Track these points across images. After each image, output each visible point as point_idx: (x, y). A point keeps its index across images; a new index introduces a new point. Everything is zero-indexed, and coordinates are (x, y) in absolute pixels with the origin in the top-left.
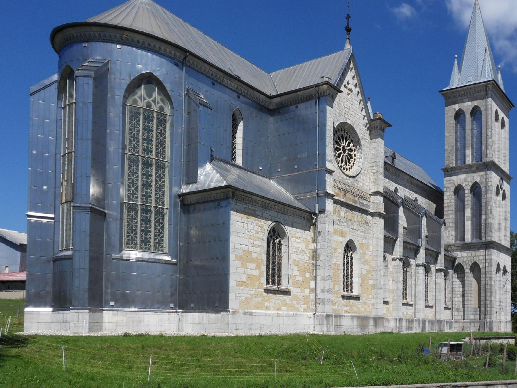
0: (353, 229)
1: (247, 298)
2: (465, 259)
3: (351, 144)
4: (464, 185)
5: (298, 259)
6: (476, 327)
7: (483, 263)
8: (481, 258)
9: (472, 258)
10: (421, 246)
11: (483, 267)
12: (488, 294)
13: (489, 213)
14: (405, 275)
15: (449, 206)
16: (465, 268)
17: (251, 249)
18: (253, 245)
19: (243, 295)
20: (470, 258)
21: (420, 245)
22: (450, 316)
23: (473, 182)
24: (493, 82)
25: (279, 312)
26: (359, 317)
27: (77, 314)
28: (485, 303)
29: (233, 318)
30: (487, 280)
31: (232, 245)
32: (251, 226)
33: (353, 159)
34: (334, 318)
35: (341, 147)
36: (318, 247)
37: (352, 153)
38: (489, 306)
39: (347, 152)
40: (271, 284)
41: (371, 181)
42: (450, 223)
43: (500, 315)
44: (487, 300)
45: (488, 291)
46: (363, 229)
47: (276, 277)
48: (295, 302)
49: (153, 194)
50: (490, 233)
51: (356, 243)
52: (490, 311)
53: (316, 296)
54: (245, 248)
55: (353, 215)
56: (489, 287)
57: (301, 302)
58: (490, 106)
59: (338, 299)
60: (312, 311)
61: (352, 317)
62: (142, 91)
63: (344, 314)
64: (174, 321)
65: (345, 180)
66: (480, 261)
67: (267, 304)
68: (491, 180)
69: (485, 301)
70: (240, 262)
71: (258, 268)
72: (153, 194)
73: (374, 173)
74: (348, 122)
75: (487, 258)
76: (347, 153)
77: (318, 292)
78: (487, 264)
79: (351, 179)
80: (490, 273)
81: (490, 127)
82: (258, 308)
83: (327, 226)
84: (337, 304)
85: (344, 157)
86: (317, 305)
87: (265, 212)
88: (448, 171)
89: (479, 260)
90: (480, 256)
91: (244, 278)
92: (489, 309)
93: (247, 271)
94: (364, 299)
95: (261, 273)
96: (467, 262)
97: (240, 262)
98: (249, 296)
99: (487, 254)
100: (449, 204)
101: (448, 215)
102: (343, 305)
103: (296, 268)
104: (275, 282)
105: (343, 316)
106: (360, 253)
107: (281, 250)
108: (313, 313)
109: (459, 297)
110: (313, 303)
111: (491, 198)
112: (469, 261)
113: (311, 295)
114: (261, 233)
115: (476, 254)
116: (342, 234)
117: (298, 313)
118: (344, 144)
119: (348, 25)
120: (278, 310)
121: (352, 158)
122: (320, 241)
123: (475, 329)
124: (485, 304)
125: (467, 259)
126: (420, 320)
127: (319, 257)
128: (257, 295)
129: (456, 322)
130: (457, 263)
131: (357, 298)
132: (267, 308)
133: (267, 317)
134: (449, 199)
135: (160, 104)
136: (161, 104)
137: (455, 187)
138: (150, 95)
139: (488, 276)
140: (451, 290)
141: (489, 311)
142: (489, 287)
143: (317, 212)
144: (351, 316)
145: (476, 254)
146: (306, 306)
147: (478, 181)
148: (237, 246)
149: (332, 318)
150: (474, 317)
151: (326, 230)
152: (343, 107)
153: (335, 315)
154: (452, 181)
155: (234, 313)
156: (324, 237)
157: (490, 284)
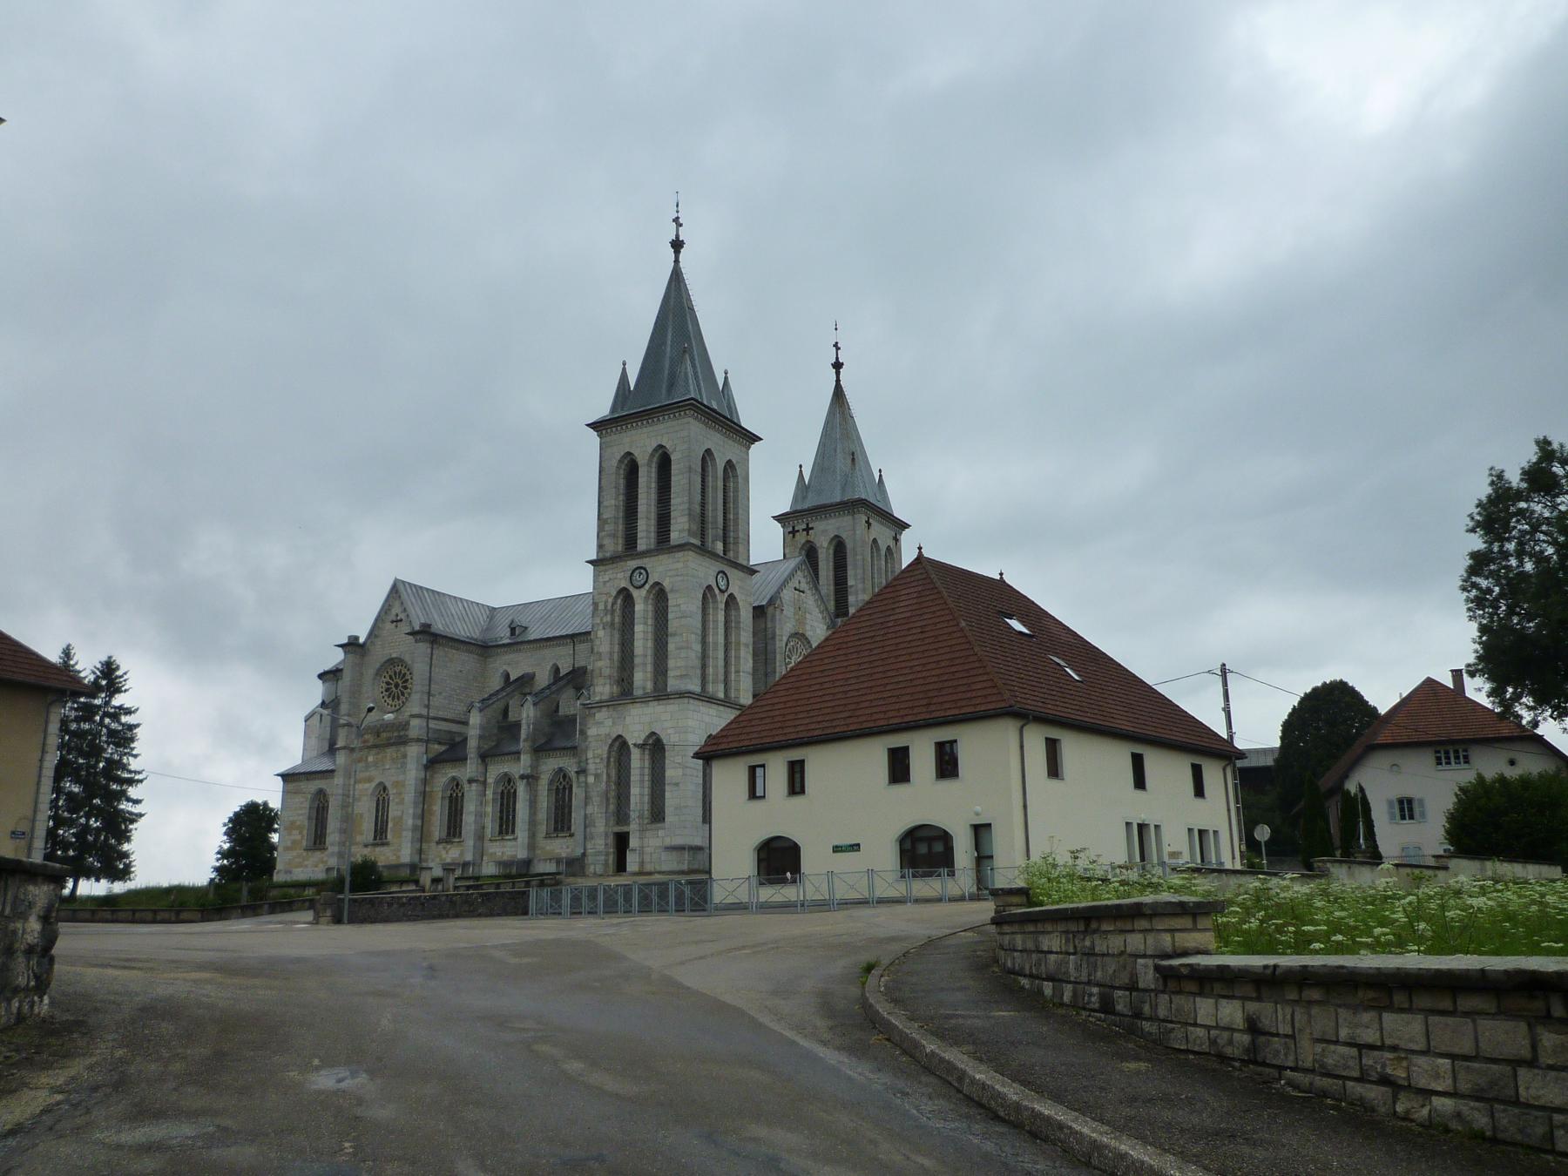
17: (295, 818)
18: (299, 815)
54: (291, 819)
67: (306, 863)
71: (301, 833)
82: (297, 867)
116: (370, 780)
132: (306, 866)
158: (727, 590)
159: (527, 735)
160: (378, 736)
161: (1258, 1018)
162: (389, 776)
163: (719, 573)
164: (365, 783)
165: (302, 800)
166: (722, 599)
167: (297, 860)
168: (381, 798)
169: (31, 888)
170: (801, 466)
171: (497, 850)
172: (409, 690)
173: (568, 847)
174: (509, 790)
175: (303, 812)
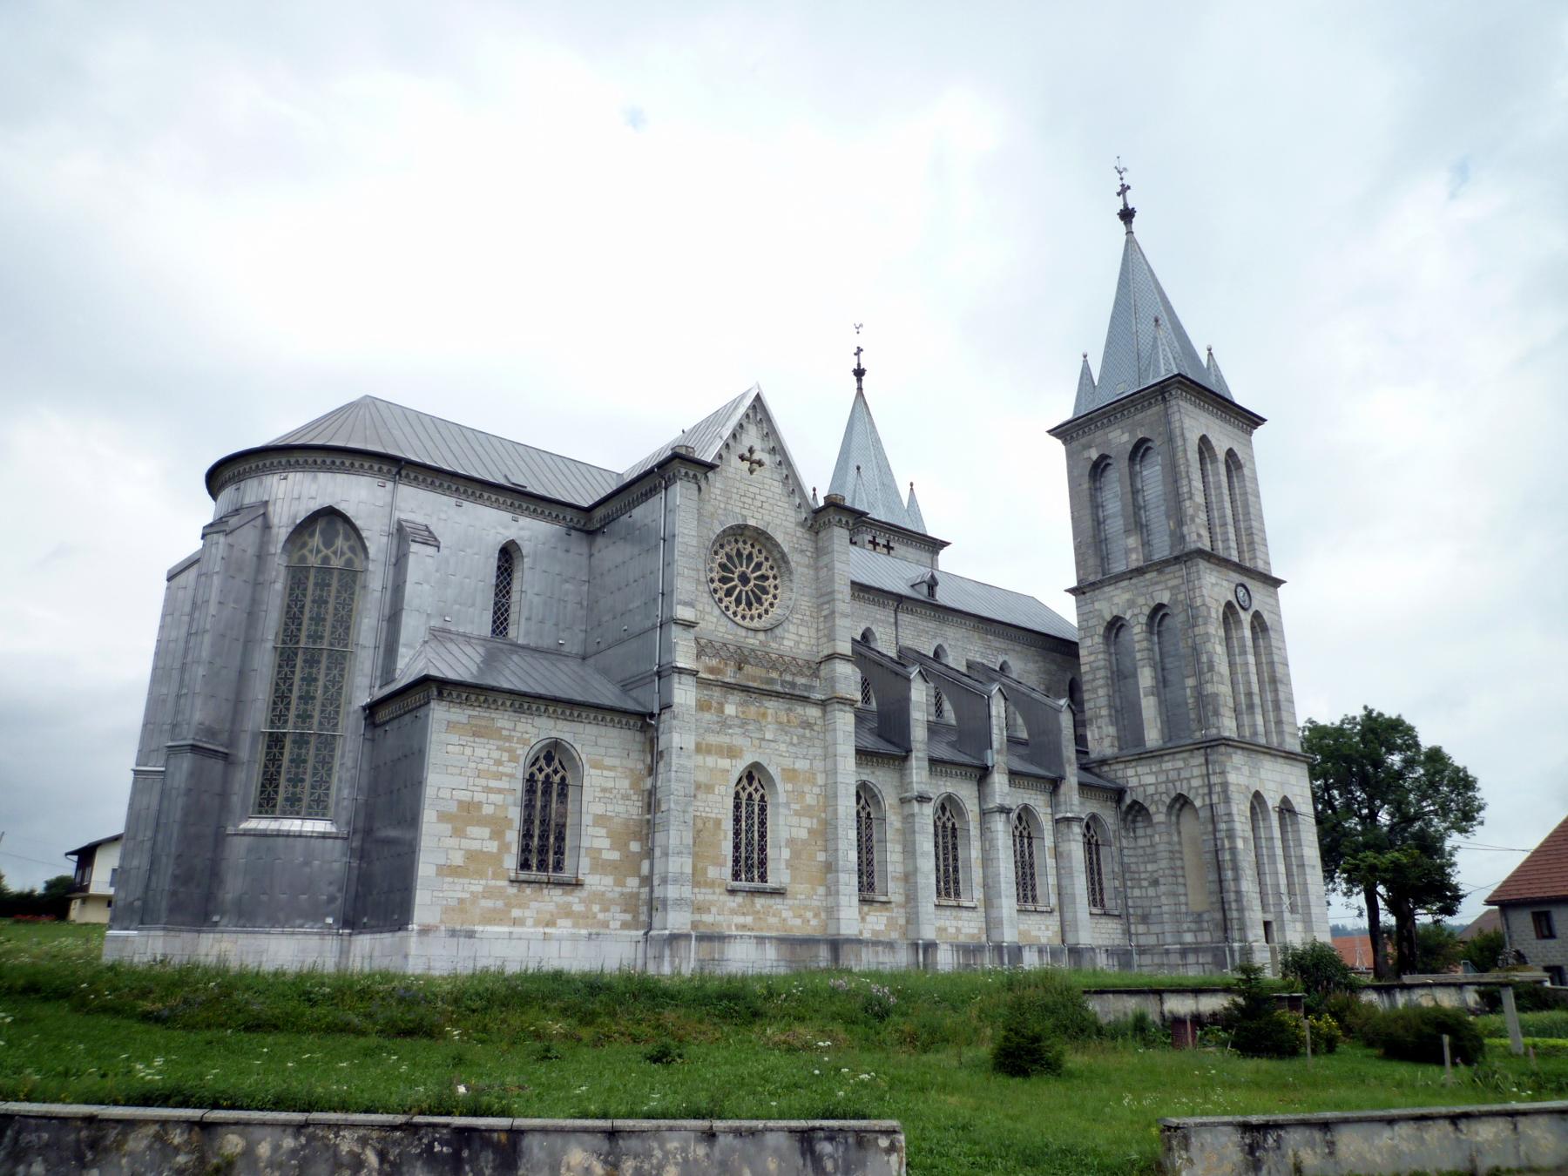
0: (763, 739)
1: (461, 901)
2: (1151, 790)
4: (1127, 617)
5: (609, 814)
6: (1203, 964)
7: (1204, 795)
8: (1196, 783)
9: (1170, 785)
10: (993, 767)
11: (1204, 806)
12: (1229, 874)
13: (1206, 670)
14: (949, 837)
15: (1094, 670)
16: (1151, 812)
17: (480, 797)
18: (488, 790)
19: (451, 894)
21: (990, 764)
22: (1120, 936)
23: (1152, 605)
24: (1180, 378)
25: (548, 930)
26: (783, 941)
27: (145, 939)
28: (1222, 898)
29: (421, 943)
30: (1222, 839)
31: (429, 792)
32: (481, 752)
33: (770, 596)
34: (693, 942)
35: (736, 576)
36: (659, 784)
37: (766, 584)
38: (1234, 906)
40: (534, 869)
41: (821, 634)
42: (1100, 708)
43: (1282, 929)
44: (1228, 892)
45: (1228, 865)
46: (795, 738)
47: (551, 853)
48: (596, 908)
49: (316, 714)
50: (1213, 720)
51: (772, 770)
52: (1239, 919)
53: (652, 891)
54: (465, 796)
55: (762, 710)
56: (1227, 857)
57: (613, 908)
59: (715, 897)
60: (643, 928)
61: (761, 940)
62: (317, 540)
63: (734, 933)
64: (331, 952)
65: (742, 640)
66: (1193, 791)
67: (516, 913)
68: (1201, 591)
69: (1221, 892)
70: (450, 826)
71: (497, 834)
72: (316, 714)
73: (825, 617)
74: (751, 522)
75: (1212, 782)
76: (752, 584)
77: (656, 882)
78: (1215, 799)
79: (761, 636)
80: (1225, 818)
81: (1184, 475)
82: (487, 920)
84: (714, 910)
85: (744, 593)
86: (654, 913)
87: (522, 720)
88: (1084, 593)
89: (1190, 788)
90: (1193, 777)
91: (458, 859)
92: (1235, 914)
93: (466, 843)
94: (803, 897)
95: (504, 847)
96: (1156, 798)
97: (450, 826)
98: (466, 895)
99: (1211, 771)
100: (1095, 665)
101: (1095, 690)
102: (733, 912)
103: (603, 832)
104: (548, 865)
105: (730, 937)
107: (566, 796)
108: (642, 932)
109: (1146, 888)
110: (644, 909)
111: (1207, 633)
112: (1161, 794)
113: (642, 890)
114: (509, 764)
115: (1179, 775)
116: (732, 752)
117: (602, 931)
118: (744, 569)
119: (859, 365)
120: (547, 925)
121: (767, 593)
123: (1201, 970)
124: (1223, 903)
125: (1156, 789)
126: (1002, 947)
127: (659, 805)
128: (488, 893)
129: (1142, 951)
130: (1128, 801)
131: (778, 893)
132: (516, 922)
133: (514, 942)
134: (1091, 654)
135: (347, 556)
136: (349, 554)
137: (1105, 624)
138: (328, 543)
139: (1223, 826)
140: (1116, 870)
141: (1235, 922)
142: (1227, 857)
143: (656, 711)
144: (756, 937)
145: (1179, 775)
146: (628, 917)
147: (1165, 601)
148: (445, 794)
149: (688, 943)
150: (1196, 936)
151: (674, 745)
152: (734, 496)
153: (696, 937)
154: (1096, 613)
155: (425, 931)
157: (1230, 849)
158: (1250, 605)
159: (1001, 744)
160: (740, 669)
161: (994, 1069)
162: (778, 756)
163: (1237, 585)
164: (722, 757)
165: (496, 754)
166: (1246, 618)
167: (487, 904)
168: (744, 796)
169: (126, 1147)
170: (912, 485)
171: (948, 923)
172: (721, 594)
173: (1047, 929)
174: (750, 795)
175: (503, 784)
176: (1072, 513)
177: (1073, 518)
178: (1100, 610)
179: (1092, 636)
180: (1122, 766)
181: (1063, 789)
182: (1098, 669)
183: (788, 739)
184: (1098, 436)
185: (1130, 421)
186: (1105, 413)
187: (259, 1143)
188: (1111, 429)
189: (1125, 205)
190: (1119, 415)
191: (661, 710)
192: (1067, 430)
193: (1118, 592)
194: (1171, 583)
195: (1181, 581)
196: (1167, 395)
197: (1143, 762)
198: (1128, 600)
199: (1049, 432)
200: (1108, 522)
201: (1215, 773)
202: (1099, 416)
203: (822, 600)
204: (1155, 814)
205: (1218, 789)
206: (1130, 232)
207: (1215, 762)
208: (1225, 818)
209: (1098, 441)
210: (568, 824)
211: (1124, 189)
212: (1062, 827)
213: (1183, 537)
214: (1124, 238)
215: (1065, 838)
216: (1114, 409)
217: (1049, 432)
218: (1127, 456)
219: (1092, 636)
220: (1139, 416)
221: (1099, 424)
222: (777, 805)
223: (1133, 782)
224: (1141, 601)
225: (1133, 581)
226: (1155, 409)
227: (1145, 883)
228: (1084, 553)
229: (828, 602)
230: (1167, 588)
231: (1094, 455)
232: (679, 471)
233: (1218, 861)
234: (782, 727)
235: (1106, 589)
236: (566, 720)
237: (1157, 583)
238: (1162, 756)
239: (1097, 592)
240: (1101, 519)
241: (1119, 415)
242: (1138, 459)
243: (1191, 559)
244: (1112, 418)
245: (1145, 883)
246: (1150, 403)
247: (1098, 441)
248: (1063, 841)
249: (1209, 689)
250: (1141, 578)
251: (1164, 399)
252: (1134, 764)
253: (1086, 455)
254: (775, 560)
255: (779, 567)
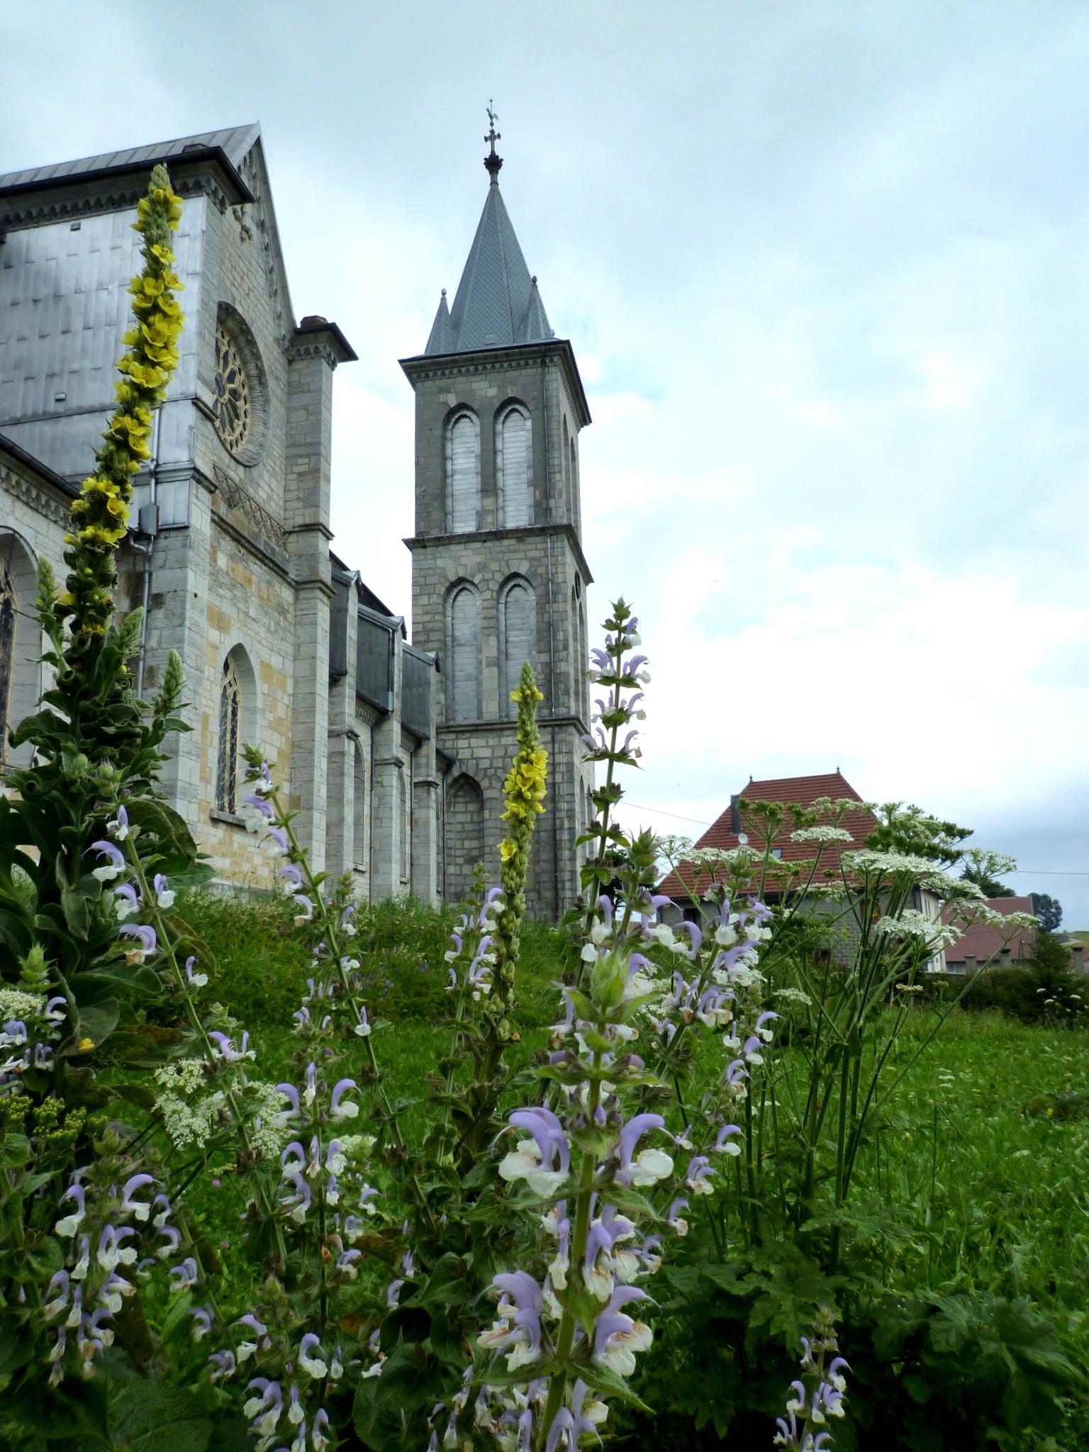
2: (484, 764)
3: (239, 378)
20: (500, 761)
21: (390, 708)
23: (507, 573)
30: (562, 819)
33: (241, 423)
38: (568, 885)
39: (227, 396)
45: (565, 845)
58: (554, 399)
69: (556, 871)
73: (300, 474)
78: (559, 778)
80: (567, 798)
83: (191, 575)
88: (425, 547)
96: (490, 772)
100: (430, 626)
106: (263, 694)
109: (461, 866)
112: (496, 769)
121: (238, 417)
122: (160, 625)
124: (556, 882)
134: (427, 613)
139: (564, 806)
151: (189, 588)
156: (177, 611)
176: (417, 457)
177: (417, 464)
178: (444, 569)
179: (429, 595)
180: (452, 736)
181: (424, 750)
182: (433, 630)
183: (266, 620)
184: (460, 382)
185: (500, 376)
186: (473, 359)
187: (1080, 1310)
188: (477, 378)
189: (493, 152)
190: (489, 366)
191: (160, 531)
192: (421, 366)
193: (469, 552)
194: (531, 554)
195: (542, 553)
196: (547, 360)
197: (480, 734)
198: (479, 564)
199: (401, 362)
200: (456, 477)
201: (560, 752)
202: (466, 360)
203: (296, 451)
204: (487, 789)
205: (563, 768)
206: (494, 183)
207: (561, 742)
208: (567, 798)
209: (458, 387)
210: (11, 682)
211: (493, 137)
212: (421, 792)
213: (548, 510)
214: (489, 187)
215: (422, 804)
216: (485, 357)
217: (401, 362)
218: (493, 412)
219: (429, 595)
220: (511, 374)
221: (463, 370)
222: (253, 710)
223: (465, 754)
224: (494, 566)
225: (488, 544)
226: (530, 371)
227: (460, 861)
228: (428, 504)
229: (307, 456)
230: (526, 558)
231: (452, 401)
232: (209, 181)
233: (555, 840)
234: (264, 603)
235: (453, 547)
236: (27, 504)
237: (514, 551)
238: (502, 730)
239: (440, 549)
240: (449, 473)
241: (489, 366)
242: (502, 418)
243: (557, 534)
244: (480, 368)
245: (460, 861)
246: (527, 364)
247: (458, 387)
248: (420, 807)
249: (562, 667)
250: (497, 543)
251: (543, 363)
252: (467, 735)
253: (442, 398)
254: (248, 376)
255: (251, 388)
